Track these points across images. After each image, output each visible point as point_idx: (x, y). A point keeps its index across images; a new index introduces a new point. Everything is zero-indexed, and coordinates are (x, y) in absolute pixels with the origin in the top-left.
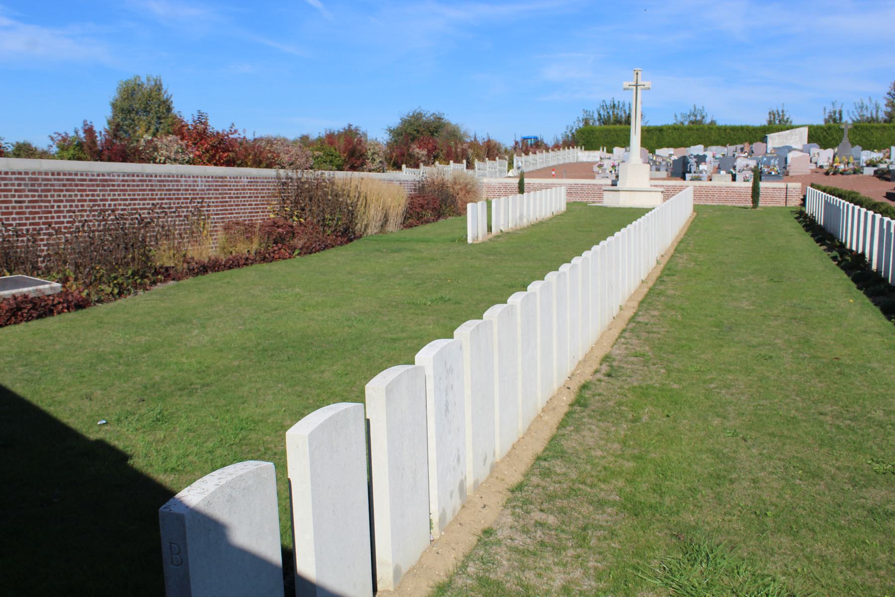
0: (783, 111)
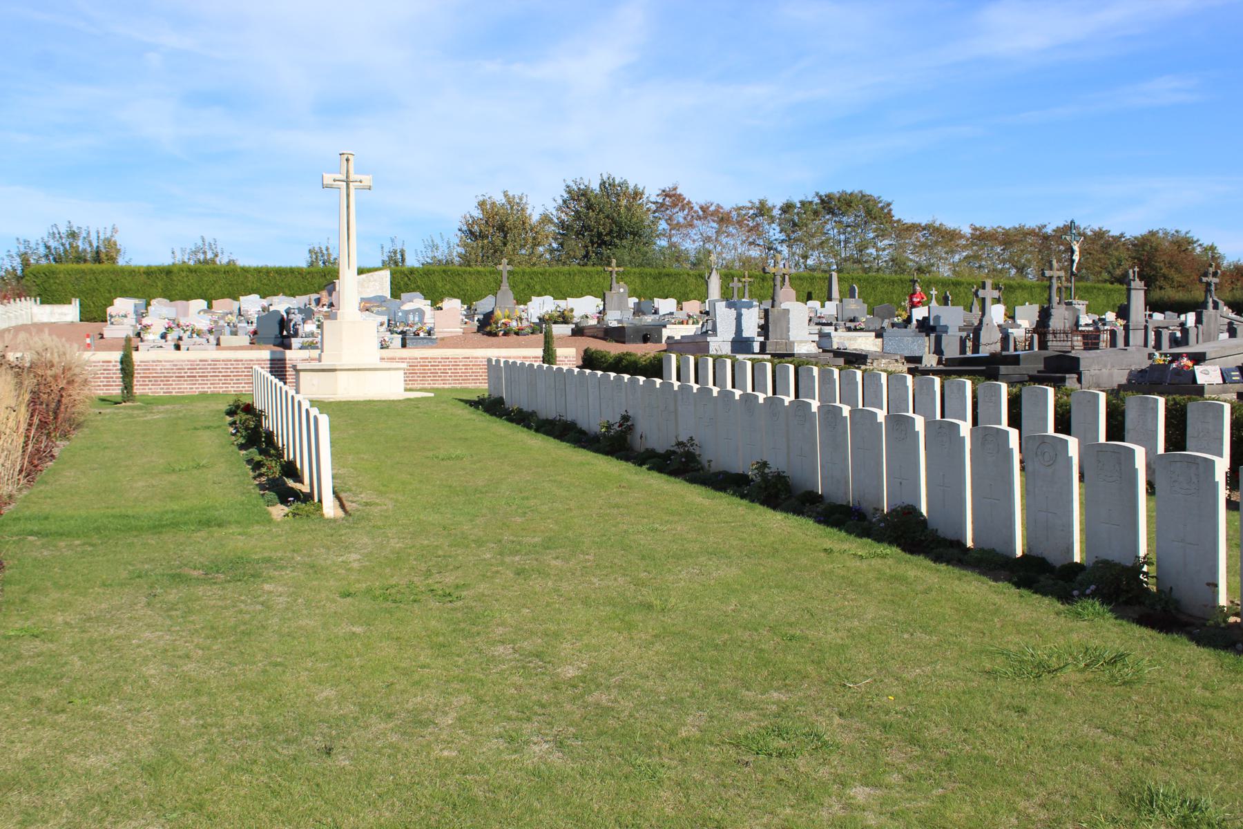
0: (327, 249)
